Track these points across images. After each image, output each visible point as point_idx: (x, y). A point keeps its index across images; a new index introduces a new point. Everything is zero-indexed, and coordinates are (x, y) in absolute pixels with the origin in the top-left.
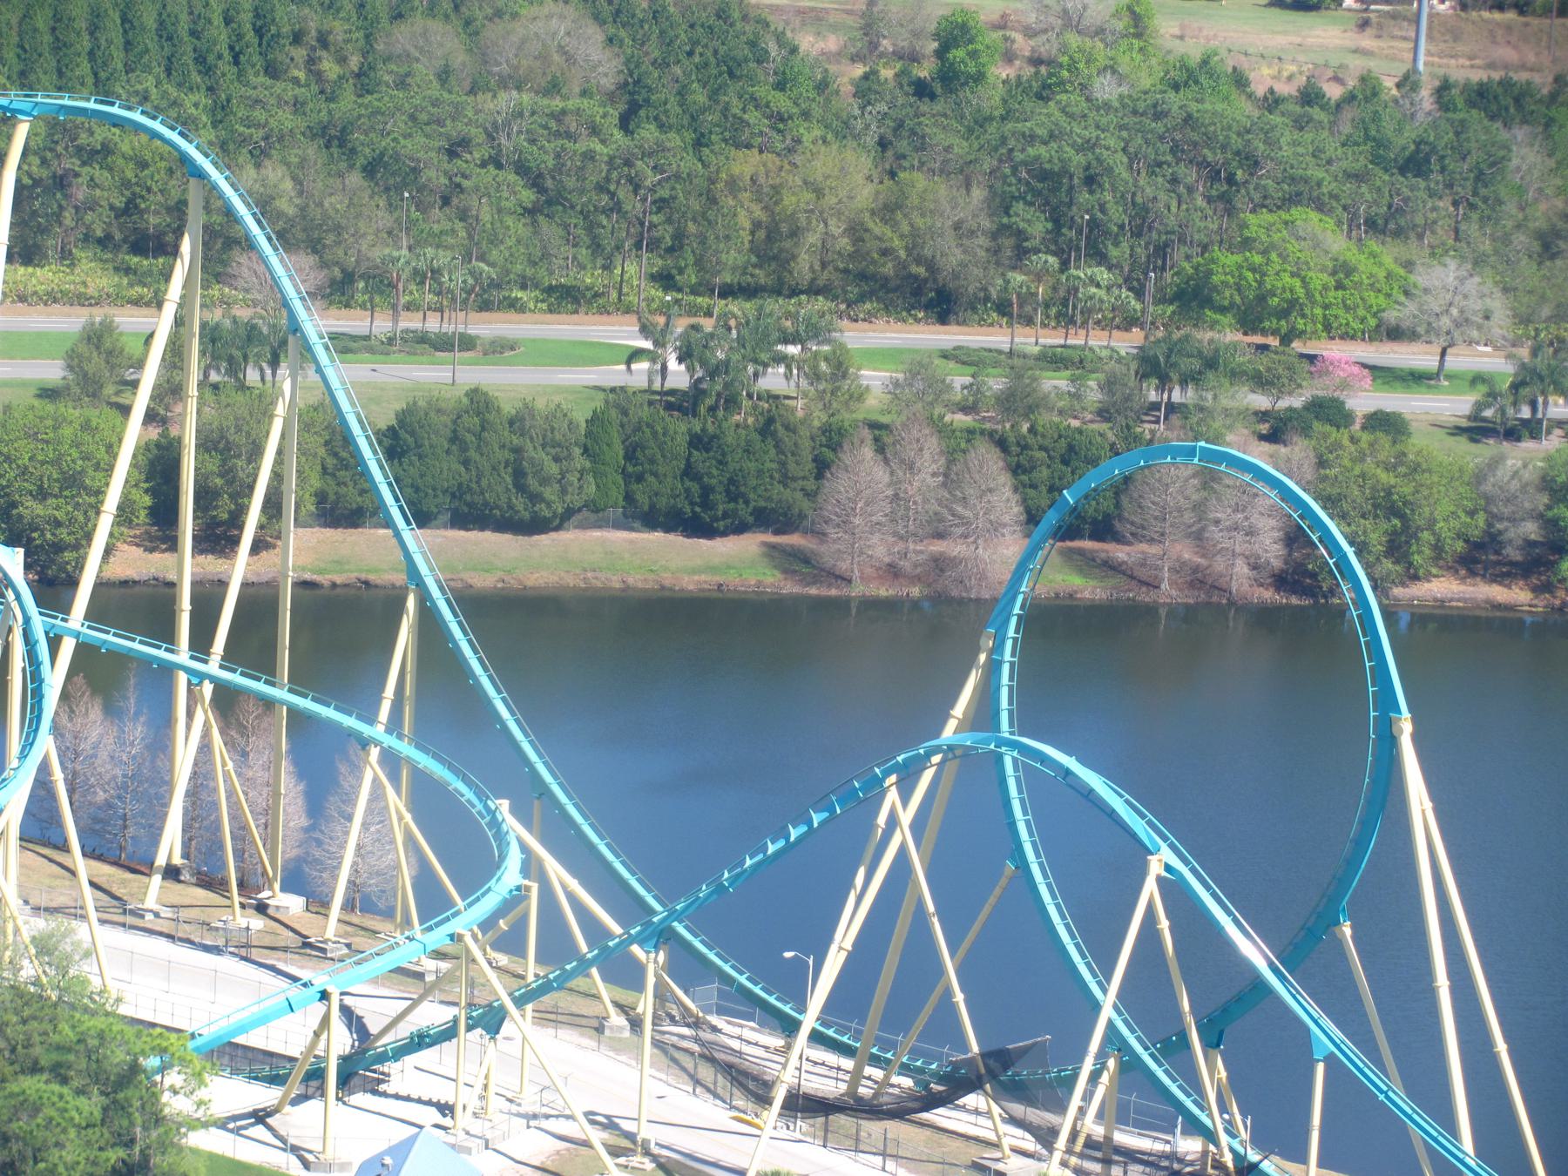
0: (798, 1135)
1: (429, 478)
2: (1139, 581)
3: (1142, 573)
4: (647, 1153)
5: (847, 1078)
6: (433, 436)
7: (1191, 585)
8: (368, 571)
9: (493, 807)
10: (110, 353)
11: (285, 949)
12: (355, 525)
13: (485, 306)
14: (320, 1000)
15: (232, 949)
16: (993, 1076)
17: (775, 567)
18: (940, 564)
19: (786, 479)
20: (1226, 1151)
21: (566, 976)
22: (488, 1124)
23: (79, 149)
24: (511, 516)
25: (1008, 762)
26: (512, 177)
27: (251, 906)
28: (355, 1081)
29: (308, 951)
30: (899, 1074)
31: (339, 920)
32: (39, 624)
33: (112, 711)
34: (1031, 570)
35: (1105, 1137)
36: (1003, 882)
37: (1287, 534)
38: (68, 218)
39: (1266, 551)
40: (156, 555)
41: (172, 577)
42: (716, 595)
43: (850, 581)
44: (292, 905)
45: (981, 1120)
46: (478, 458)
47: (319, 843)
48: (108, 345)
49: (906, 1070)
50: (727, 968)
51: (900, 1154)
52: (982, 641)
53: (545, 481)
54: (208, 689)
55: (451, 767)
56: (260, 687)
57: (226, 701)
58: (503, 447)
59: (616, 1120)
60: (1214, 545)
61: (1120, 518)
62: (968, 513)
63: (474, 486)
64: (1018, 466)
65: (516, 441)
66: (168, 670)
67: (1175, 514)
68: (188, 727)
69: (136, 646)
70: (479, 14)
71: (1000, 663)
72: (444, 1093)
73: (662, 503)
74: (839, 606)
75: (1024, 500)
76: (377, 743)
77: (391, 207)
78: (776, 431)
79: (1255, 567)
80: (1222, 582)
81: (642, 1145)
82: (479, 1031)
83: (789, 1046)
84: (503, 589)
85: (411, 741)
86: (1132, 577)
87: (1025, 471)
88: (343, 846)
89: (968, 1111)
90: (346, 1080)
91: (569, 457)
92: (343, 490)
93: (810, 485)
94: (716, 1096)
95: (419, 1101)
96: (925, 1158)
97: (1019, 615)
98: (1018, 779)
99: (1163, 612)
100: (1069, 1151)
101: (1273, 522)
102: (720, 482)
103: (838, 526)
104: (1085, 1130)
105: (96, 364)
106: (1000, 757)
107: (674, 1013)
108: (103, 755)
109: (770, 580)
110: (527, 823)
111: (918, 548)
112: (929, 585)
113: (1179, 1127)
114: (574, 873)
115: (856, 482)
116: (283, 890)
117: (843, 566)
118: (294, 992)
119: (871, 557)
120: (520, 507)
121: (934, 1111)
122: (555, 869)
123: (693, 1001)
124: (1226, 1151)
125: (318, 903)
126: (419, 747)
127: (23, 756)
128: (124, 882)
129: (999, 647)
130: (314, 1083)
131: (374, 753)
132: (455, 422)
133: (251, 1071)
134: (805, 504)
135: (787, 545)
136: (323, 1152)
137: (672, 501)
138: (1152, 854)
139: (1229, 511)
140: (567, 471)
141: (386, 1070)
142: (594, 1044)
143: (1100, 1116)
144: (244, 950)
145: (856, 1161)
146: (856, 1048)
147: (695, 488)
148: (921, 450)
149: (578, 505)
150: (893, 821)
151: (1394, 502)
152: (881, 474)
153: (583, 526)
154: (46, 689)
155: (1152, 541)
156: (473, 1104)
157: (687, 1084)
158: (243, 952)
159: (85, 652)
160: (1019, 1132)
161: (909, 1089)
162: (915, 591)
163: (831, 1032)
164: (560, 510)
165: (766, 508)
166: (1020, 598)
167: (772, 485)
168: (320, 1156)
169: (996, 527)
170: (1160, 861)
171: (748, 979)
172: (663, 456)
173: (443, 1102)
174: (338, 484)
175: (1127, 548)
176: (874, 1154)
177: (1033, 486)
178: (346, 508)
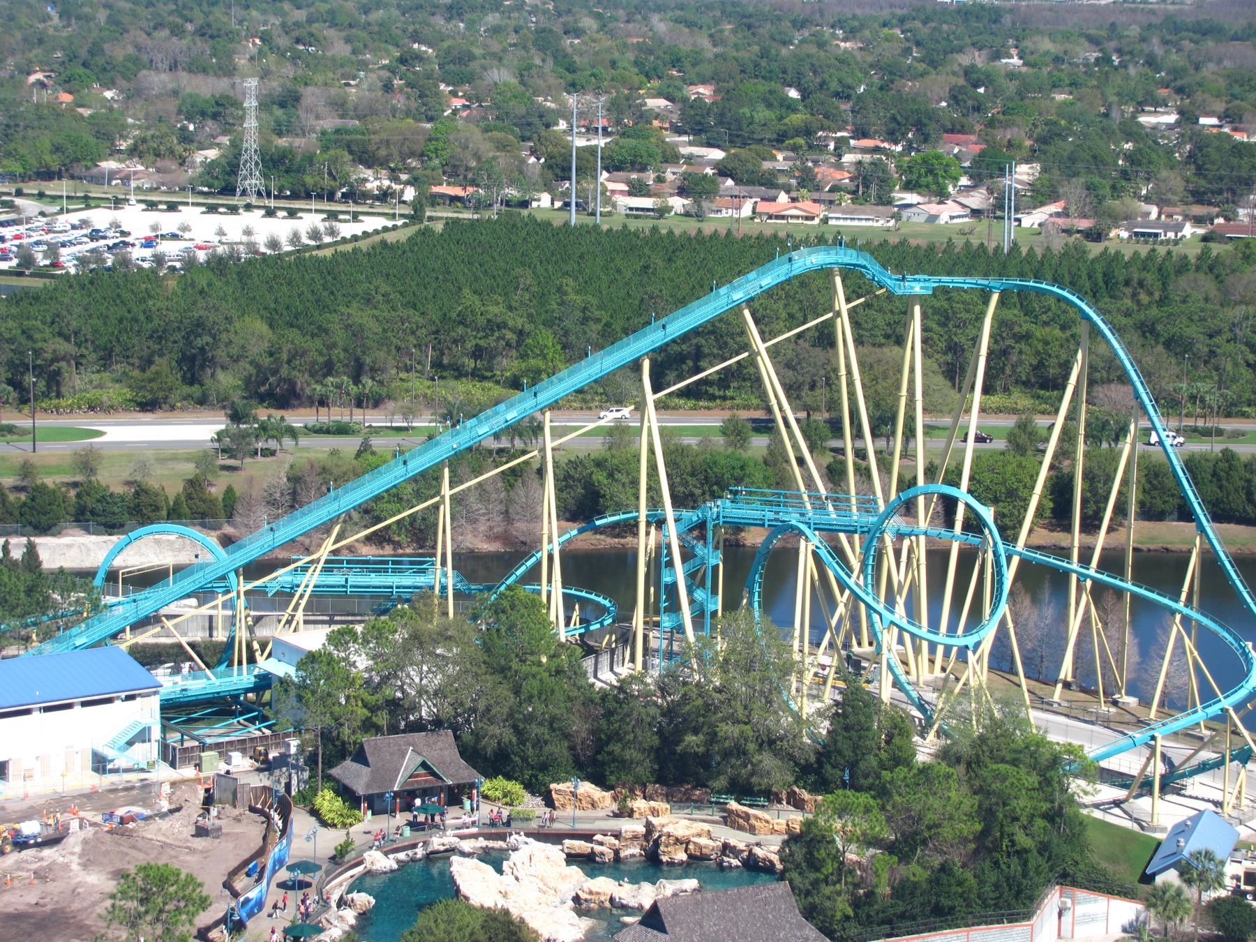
10: (1030, 434)
11: (1128, 723)
12: (1161, 520)
13: (1228, 415)
23: (1014, 336)
26: (1243, 348)
28: (1168, 789)
32: (1001, 548)
33: (1035, 600)
38: (1008, 371)
40: (1055, 534)
41: (1064, 544)
44: (1132, 701)
47: (1146, 670)
48: (1029, 429)
54: (1089, 583)
56: (1117, 582)
57: (1099, 590)
65: (1248, 476)
66: (1066, 574)
68: (1076, 610)
69: (1051, 560)
70: (1224, 273)
72: (1217, 796)
76: (1180, 612)
77: (1179, 364)
82: (1236, 762)
88: (1159, 672)
90: (1164, 789)
95: (1203, 799)
105: (1023, 439)
108: (1031, 624)
116: (1127, 694)
125: (1146, 702)
126: (1203, 614)
127: (992, 613)
128: (1041, 689)
131: (1178, 617)
144: (1106, 723)
154: (1005, 580)
156: (1233, 801)
159: (1025, 564)
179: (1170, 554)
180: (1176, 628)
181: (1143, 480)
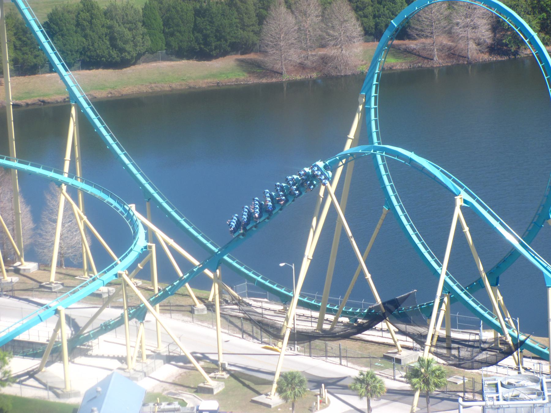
0: (296, 352)
1: (68, 46)
2: (423, 57)
3: (424, 54)
4: (224, 370)
5: (317, 320)
6: (67, 25)
7: (449, 56)
8: (44, 96)
9: (128, 209)
11: (31, 290)
14: (55, 314)
15: (5, 293)
16: (390, 312)
17: (244, 71)
18: (325, 60)
19: (244, 27)
20: (508, 336)
21: (174, 288)
22: (144, 365)
24: (111, 61)
25: (379, 158)
27: (11, 270)
29: (43, 289)
30: (342, 316)
31: (56, 273)
34: (380, 61)
35: (447, 336)
36: (383, 217)
37: (492, 26)
39: (483, 35)
42: (217, 88)
43: (281, 74)
44: (31, 267)
45: (385, 334)
46: (91, 33)
49: (345, 314)
50: (251, 274)
51: (348, 356)
52: (360, 99)
53: (126, 42)
55: (104, 192)
58: (103, 26)
59: (207, 355)
60: (458, 36)
61: (409, 26)
62: (336, 34)
63: (91, 47)
64: (357, 7)
65: (109, 22)
67: (437, 22)
71: (369, 109)
72: (121, 352)
73: (185, 45)
74: (278, 87)
75: (362, 24)
76: (66, 184)
78: (236, 3)
79: (478, 44)
80: (463, 53)
81: (222, 366)
82: (135, 320)
83: (285, 310)
84: (111, 97)
85: (82, 181)
86: (419, 56)
87: (361, 10)
89: (378, 330)
91: (136, 28)
92: (26, 56)
93: (256, 28)
94: (254, 337)
95: (108, 357)
96: (360, 356)
97: (376, 85)
98: (384, 165)
99: (436, 72)
100: (432, 346)
101: (485, 21)
102: (212, 32)
103: (273, 47)
104: (437, 334)
106: (374, 156)
107: (227, 299)
109: (242, 78)
110: (144, 213)
111: (313, 53)
112: (321, 71)
113: (482, 326)
114: (171, 237)
115: (279, 25)
116: (26, 260)
117: (278, 67)
118: (40, 311)
119: (291, 61)
120: (115, 56)
121: (363, 333)
122: (161, 235)
123: (236, 292)
124: (508, 336)
125: (45, 265)
126: (87, 183)
129: (368, 101)
130: (55, 355)
131: (64, 187)
132: (77, 17)
133: (23, 352)
134: (255, 38)
135: (249, 59)
136: (65, 388)
137: (189, 44)
138: (457, 196)
139: (463, 18)
140: (136, 35)
141: (90, 344)
142: (190, 319)
143: (443, 325)
145: (327, 362)
146: (319, 306)
147: (200, 36)
148: (309, 5)
149: (143, 51)
150: (327, 192)
151: (542, 5)
152: (291, 19)
153: (147, 61)
155: (427, 37)
157: (239, 334)
158: (10, 293)
160: (404, 338)
161: (347, 323)
162: (314, 75)
163: (305, 300)
164: (135, 55)
165: (236, 42)
166: (376, 76)
167: (237, 30)
168: (64, 390)
169: (350, 39)
170: (461, 198)
171: (262, 278)
172: (183, 22)
173: (120, 356)
174: (23, 54)
175: (415, 42)
176: (335, 357)
177: (366, 16)
178: (28, 66)
179: (46, 106)
180: (64, 197)
181: (13, 39)
